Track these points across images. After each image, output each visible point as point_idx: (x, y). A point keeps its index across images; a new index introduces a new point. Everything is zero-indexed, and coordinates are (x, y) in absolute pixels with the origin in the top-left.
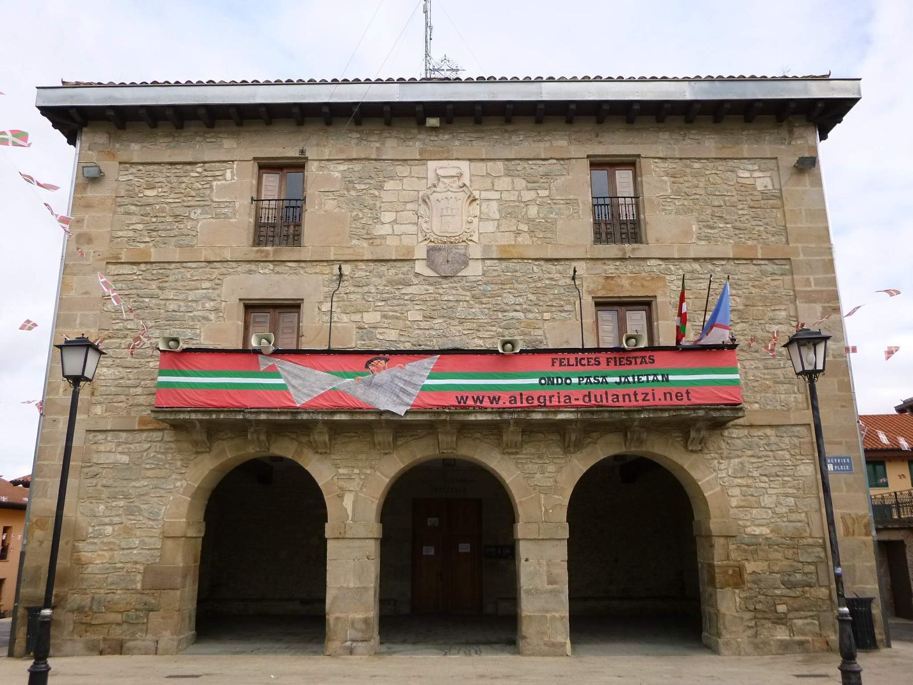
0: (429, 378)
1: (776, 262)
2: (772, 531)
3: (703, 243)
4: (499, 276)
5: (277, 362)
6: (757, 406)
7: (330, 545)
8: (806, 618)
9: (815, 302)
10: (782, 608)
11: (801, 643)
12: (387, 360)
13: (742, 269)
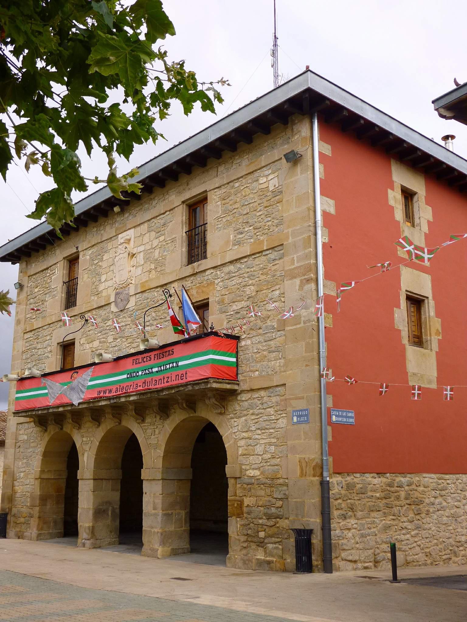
0: (90, 381)
1: (276, 249)
2: (262, 473)
3: (236, 247)
4: (142, 304)
5: (43, 380)
6: (257, 373)
7: (80, 483)
8: (275, 543)
9: (295, 278)
10: (262, 534)
11: (269, 563)
12: (77, 373)
13: (257, 261)
